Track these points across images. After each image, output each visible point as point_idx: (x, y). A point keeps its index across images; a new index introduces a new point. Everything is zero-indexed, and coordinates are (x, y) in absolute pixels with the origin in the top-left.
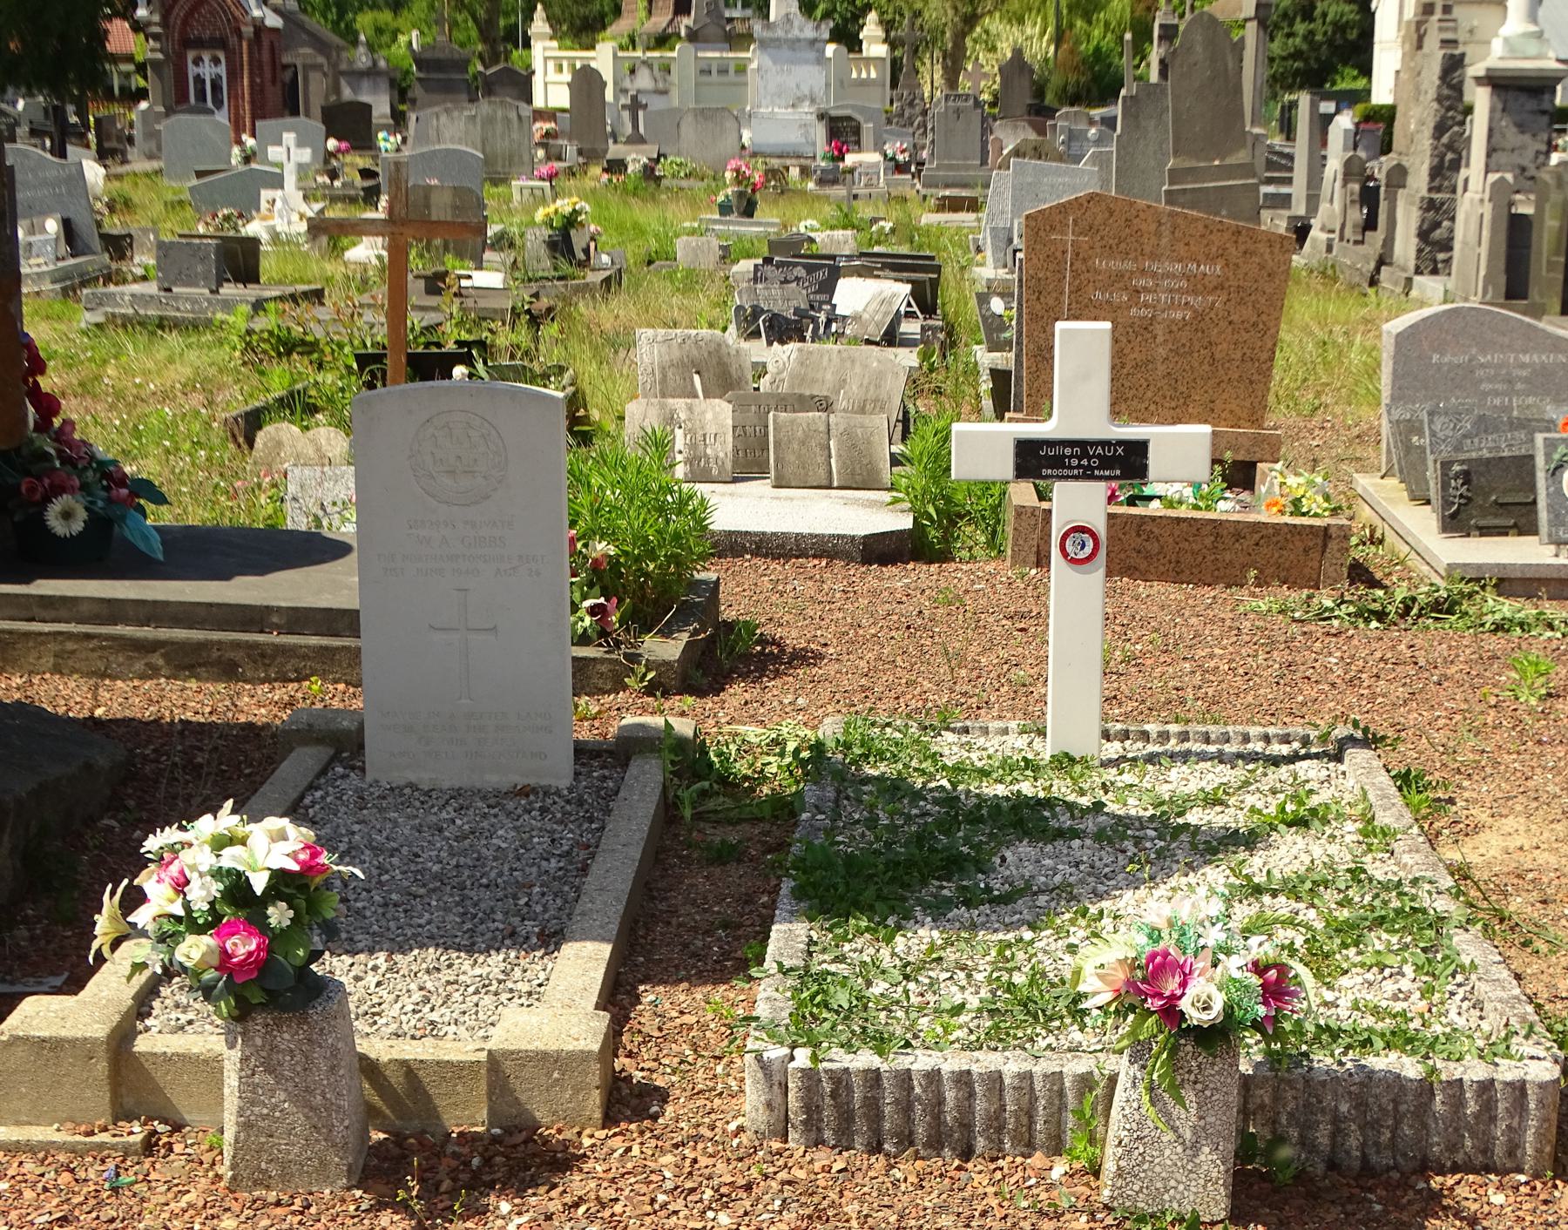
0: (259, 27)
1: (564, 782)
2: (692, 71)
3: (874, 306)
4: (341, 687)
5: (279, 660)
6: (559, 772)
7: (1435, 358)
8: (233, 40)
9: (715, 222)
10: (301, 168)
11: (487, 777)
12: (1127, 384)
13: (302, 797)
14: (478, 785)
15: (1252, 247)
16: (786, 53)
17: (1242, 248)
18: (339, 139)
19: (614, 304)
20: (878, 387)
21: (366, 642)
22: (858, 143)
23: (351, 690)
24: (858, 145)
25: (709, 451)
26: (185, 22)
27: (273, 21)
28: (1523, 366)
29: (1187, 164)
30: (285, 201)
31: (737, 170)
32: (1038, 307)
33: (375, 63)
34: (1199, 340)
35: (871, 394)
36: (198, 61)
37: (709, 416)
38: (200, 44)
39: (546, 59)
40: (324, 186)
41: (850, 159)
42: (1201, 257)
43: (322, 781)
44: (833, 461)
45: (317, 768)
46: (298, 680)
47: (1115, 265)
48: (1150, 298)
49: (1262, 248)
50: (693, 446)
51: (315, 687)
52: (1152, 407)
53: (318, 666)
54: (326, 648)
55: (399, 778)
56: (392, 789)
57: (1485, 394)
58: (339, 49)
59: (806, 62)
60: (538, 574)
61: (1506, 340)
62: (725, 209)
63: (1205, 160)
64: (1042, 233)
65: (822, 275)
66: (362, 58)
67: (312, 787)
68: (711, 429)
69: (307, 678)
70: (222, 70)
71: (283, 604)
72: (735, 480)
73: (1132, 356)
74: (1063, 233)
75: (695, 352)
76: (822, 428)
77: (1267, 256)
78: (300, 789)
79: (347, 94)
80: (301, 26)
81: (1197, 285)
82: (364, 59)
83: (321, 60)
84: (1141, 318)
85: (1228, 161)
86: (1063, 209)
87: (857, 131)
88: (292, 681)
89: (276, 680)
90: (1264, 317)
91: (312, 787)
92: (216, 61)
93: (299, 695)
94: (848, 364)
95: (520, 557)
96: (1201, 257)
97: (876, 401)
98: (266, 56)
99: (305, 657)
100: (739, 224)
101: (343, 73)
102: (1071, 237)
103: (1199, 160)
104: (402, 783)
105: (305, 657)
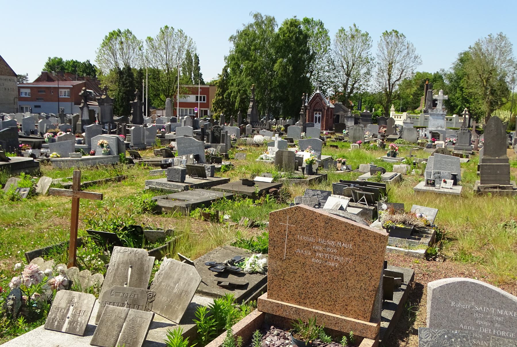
0: (329, 108)
2: (423, 119)
3: (335, 207)
7: (453, 304)
8: (323, 110)
9: (385, 158)
12: (310, 291)
15: (367, 239)
16: (436, 117)
17: (362, 238)
19: (320, 185)
20: (189, 285)
22: (439, 139)
24: (439, 139)
25: (79, 319)
26: (314, 106)
27: (332, 106)
28: (499, 315)
29: (488, 158)
31: (392, 146)
32: (274, 253)
34: (342, 277)
35: (185, 289)
36: (316, 114)
37: (85, 302)
38: (317, 110)
41: (436, 142)
42: (343, 240)
44: (121, 334)
47: (306, 239)
48: (320, 255)
49: (371, 239)
50: (74, 315)
52: (320, 303)
57: (479, 326)
59: (440, 119)
61: (490, 302)
62: (388, 155)
64: (276, 222)
65: (325, 194)
66: (349, 114)
68: (84, 308)
70: (321, 115)
72: (83, 336)
73: (312, 280)
75: (133, 258)
76: (123, 316)
77: (373, 243)
81: (341, 252)
84: (316, 263)
85: (500, 158)
87: (439, 136)
90: (371, 271)
92: (319, 114)
94: (183, 272)
96: (343, 240)
97: (186, 291)
98: (329, 113)
100: (387, 158)
102: (288, 224)
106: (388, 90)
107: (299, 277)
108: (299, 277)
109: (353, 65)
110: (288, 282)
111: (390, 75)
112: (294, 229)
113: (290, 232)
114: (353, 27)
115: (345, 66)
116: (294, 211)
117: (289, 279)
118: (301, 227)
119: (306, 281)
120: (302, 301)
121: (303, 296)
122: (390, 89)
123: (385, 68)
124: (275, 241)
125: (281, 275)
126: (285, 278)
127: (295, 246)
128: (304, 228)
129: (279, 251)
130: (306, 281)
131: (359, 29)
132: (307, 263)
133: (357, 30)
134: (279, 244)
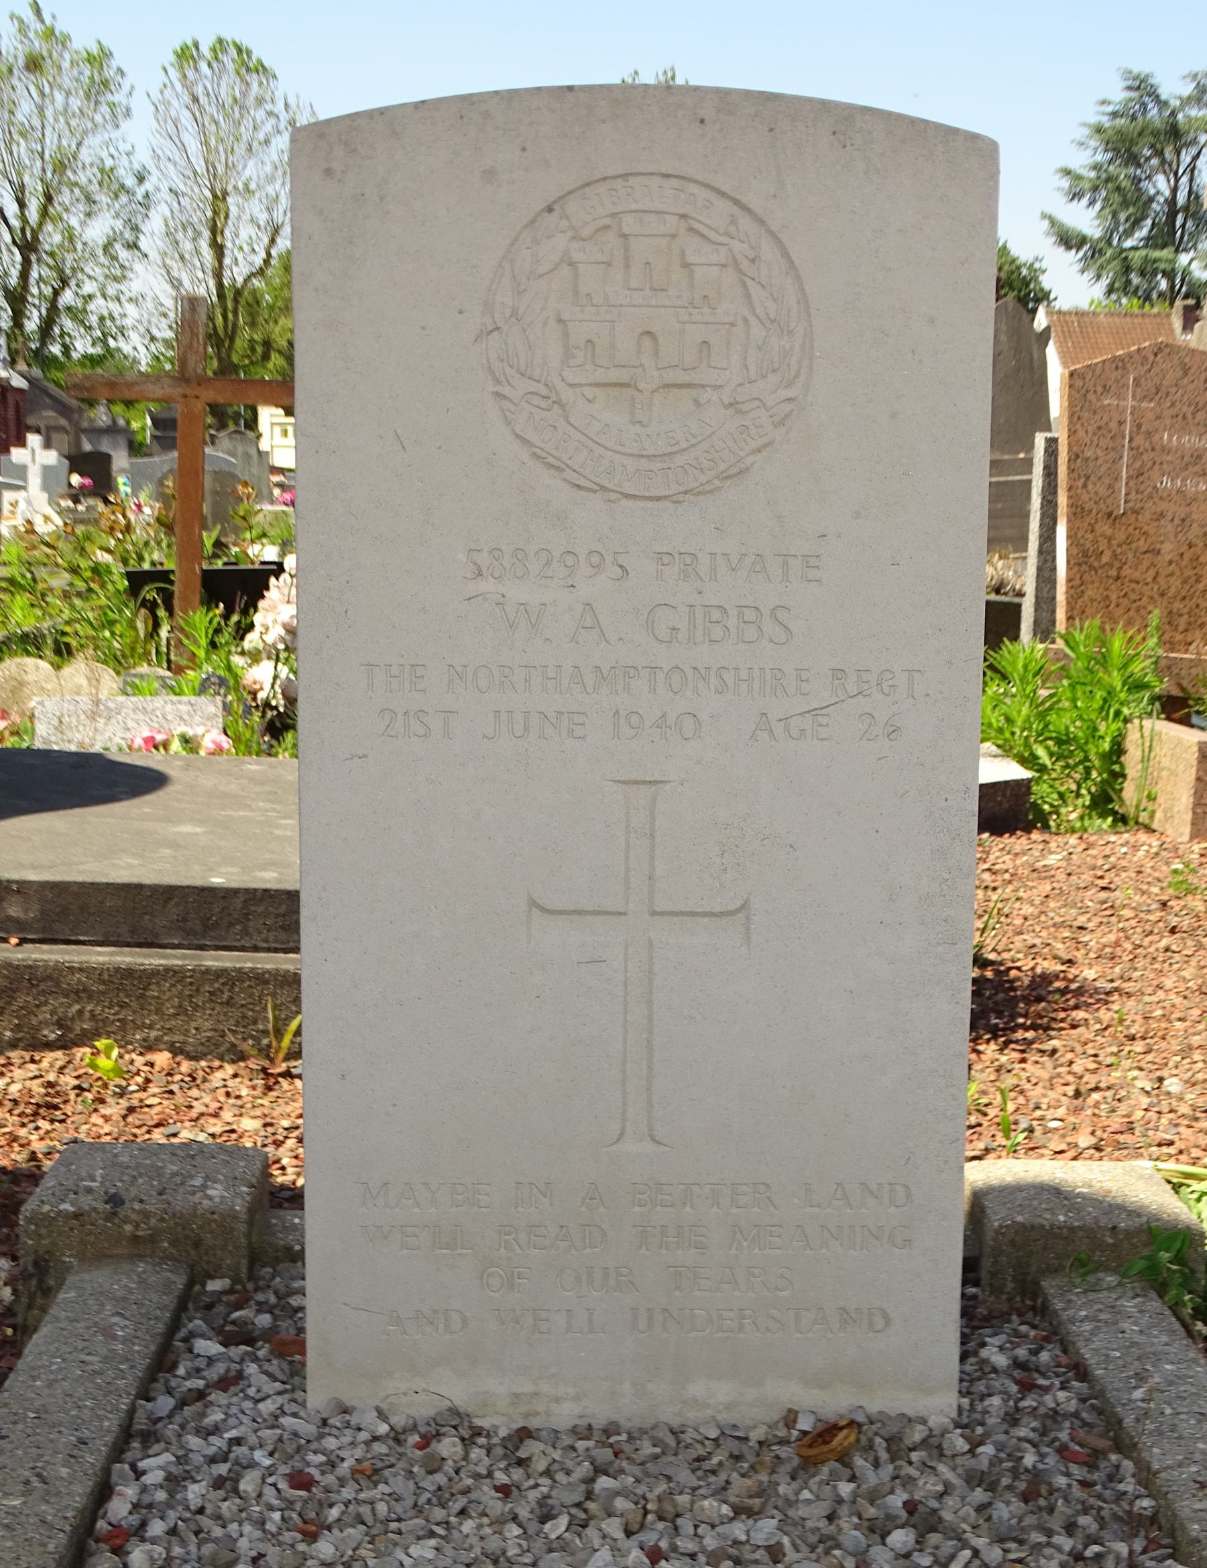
1: (940, 1404)
4: (162, 1058)
5: (21, 999)
6: (904, 1350)
10: (46, 470)
11: (696, 1389)
13: (103, 1492)
14: (670, 1415)
18: (81, 475)
21: (318, 958)
23: (186, 1066)
30: (29, 502)
33: (114, 422)
39: (273, 424)
40: (69, 510)
43: (164, 1404)
45: (143, 1351)
46: (64, 1044)
51: (104, 1063)
53: (109, 1013)
54: (128, 973)
55: (416, 1396)
56: (397, 1436)
58: (80, 410)
60: (893, 731)
63: (1009, 453)
67: (132, 1437)
69: (85, 1039)
71: (32, 876)
74: (1120, 397)
78: (92, 1459)
79: (87, 447)
80: (45, 392)
82: (105, 418)
83: (63, 422)
86: (1120, 364)
88: (50, 1046)
89: (14, 1045)
91: (132, 1437)
93: (68, 1081)
95: (839, 673)
99: (80, 993)
101: (84, 431)
103: (1003, 453)
104: (423, 1409)
105: (80, 993)
106: (219, 320)
107: (1170, 562)
108: (1170, 562)
109: (49, 198)
110: (1133, 585)
111: (219, 250)
112: (1151, 415)
113: (1139, 426)
114: (28, 15)
115: (11, 209)
116: (1151, 358)
117: (1137, 575)
118: (1173, 404)
119: (1191, 573)
120: (1178, 637)
121: (1182, 622)
122: (225, 317)
123: (201, 217)
124: (1087, 460)
125: (1111, 565)
126: (1123, 573)
127: (1157, 467)
128: (1185, 409)
129: (1102, 491)
130: (1191, 573)
131: (60, 27)
132: (1194, 516)
133: (50, 33)
134: (1103, 469)
